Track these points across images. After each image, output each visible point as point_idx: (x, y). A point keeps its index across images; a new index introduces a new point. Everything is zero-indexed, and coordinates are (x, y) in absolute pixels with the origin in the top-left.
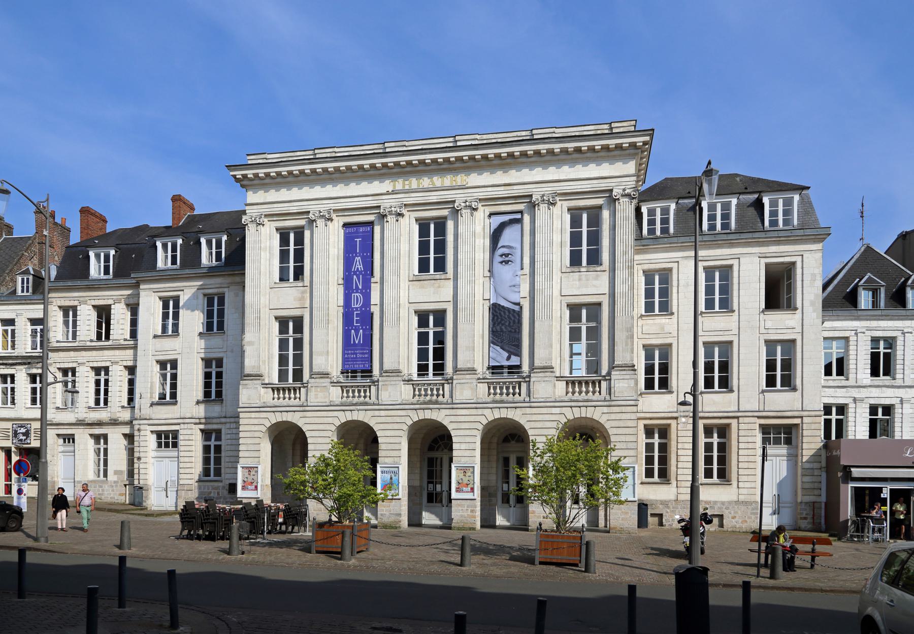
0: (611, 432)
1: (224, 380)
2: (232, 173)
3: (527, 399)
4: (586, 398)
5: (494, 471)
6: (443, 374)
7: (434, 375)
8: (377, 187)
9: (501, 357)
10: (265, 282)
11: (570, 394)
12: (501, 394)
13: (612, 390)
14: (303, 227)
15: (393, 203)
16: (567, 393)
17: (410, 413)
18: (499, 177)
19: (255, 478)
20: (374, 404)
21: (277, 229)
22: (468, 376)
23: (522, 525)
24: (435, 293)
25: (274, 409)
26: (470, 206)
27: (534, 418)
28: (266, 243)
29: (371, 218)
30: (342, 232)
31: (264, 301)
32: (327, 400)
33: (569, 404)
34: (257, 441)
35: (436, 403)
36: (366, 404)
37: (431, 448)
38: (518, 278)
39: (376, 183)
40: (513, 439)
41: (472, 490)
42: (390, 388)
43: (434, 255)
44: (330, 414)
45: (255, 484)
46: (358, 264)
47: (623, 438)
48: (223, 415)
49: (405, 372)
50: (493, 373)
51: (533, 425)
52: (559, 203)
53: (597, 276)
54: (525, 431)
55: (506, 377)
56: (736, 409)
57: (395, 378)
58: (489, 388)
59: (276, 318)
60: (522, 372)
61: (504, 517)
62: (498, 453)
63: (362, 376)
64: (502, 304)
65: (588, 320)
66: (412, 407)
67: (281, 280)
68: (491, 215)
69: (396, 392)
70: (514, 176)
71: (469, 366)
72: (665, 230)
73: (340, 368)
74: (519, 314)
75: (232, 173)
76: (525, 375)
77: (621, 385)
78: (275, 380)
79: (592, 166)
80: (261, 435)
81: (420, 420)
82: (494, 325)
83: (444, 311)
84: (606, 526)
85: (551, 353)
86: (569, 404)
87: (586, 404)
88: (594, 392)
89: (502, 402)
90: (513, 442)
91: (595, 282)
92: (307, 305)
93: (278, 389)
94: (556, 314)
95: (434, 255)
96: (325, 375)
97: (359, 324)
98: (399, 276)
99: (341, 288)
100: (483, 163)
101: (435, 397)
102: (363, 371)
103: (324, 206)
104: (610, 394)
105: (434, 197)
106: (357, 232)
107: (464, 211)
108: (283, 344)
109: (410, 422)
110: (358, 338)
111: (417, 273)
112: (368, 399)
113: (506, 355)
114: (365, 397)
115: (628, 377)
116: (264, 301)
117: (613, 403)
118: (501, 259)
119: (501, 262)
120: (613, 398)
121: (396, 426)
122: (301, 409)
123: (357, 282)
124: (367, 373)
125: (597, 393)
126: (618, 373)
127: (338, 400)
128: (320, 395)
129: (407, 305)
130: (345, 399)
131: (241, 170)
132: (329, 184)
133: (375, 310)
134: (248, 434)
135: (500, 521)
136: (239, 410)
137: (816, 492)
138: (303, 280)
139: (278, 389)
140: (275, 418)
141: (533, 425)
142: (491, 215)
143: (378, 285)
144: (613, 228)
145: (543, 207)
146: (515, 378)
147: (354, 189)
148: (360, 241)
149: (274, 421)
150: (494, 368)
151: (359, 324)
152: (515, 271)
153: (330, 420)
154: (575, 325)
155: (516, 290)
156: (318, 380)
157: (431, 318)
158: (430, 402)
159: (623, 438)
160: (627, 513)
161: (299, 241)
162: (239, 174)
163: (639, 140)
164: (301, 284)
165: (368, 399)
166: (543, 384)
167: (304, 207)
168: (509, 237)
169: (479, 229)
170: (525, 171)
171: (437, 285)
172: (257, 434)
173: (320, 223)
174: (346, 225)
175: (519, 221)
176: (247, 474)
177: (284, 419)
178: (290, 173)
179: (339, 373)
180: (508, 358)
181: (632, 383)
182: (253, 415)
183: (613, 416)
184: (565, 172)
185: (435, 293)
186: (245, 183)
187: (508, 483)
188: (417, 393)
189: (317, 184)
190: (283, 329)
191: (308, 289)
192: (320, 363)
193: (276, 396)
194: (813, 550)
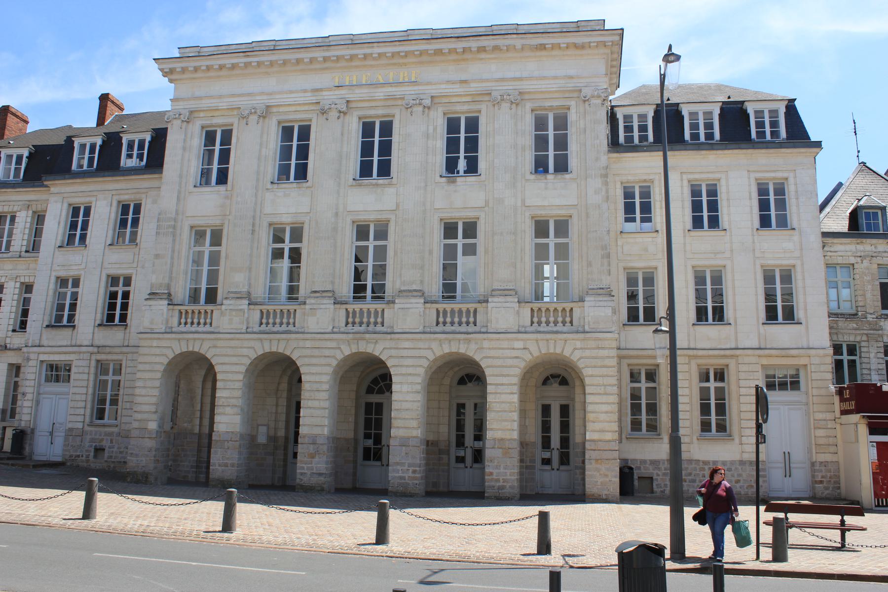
1: (131, 302)
4: (287, 329)
11: (535, 324)
37: (370, 391)
47: (600, 380)
51: (307, 361)
72: (709, 136)
114: (288, 324)
115: (605, 304)
121: (234, 360)
125: (568, 324)
126: (592, 299)
137: (833, 449)
141: (307, 361)
145: (505, 106)
159: (600, 380)
194: (843, 522)
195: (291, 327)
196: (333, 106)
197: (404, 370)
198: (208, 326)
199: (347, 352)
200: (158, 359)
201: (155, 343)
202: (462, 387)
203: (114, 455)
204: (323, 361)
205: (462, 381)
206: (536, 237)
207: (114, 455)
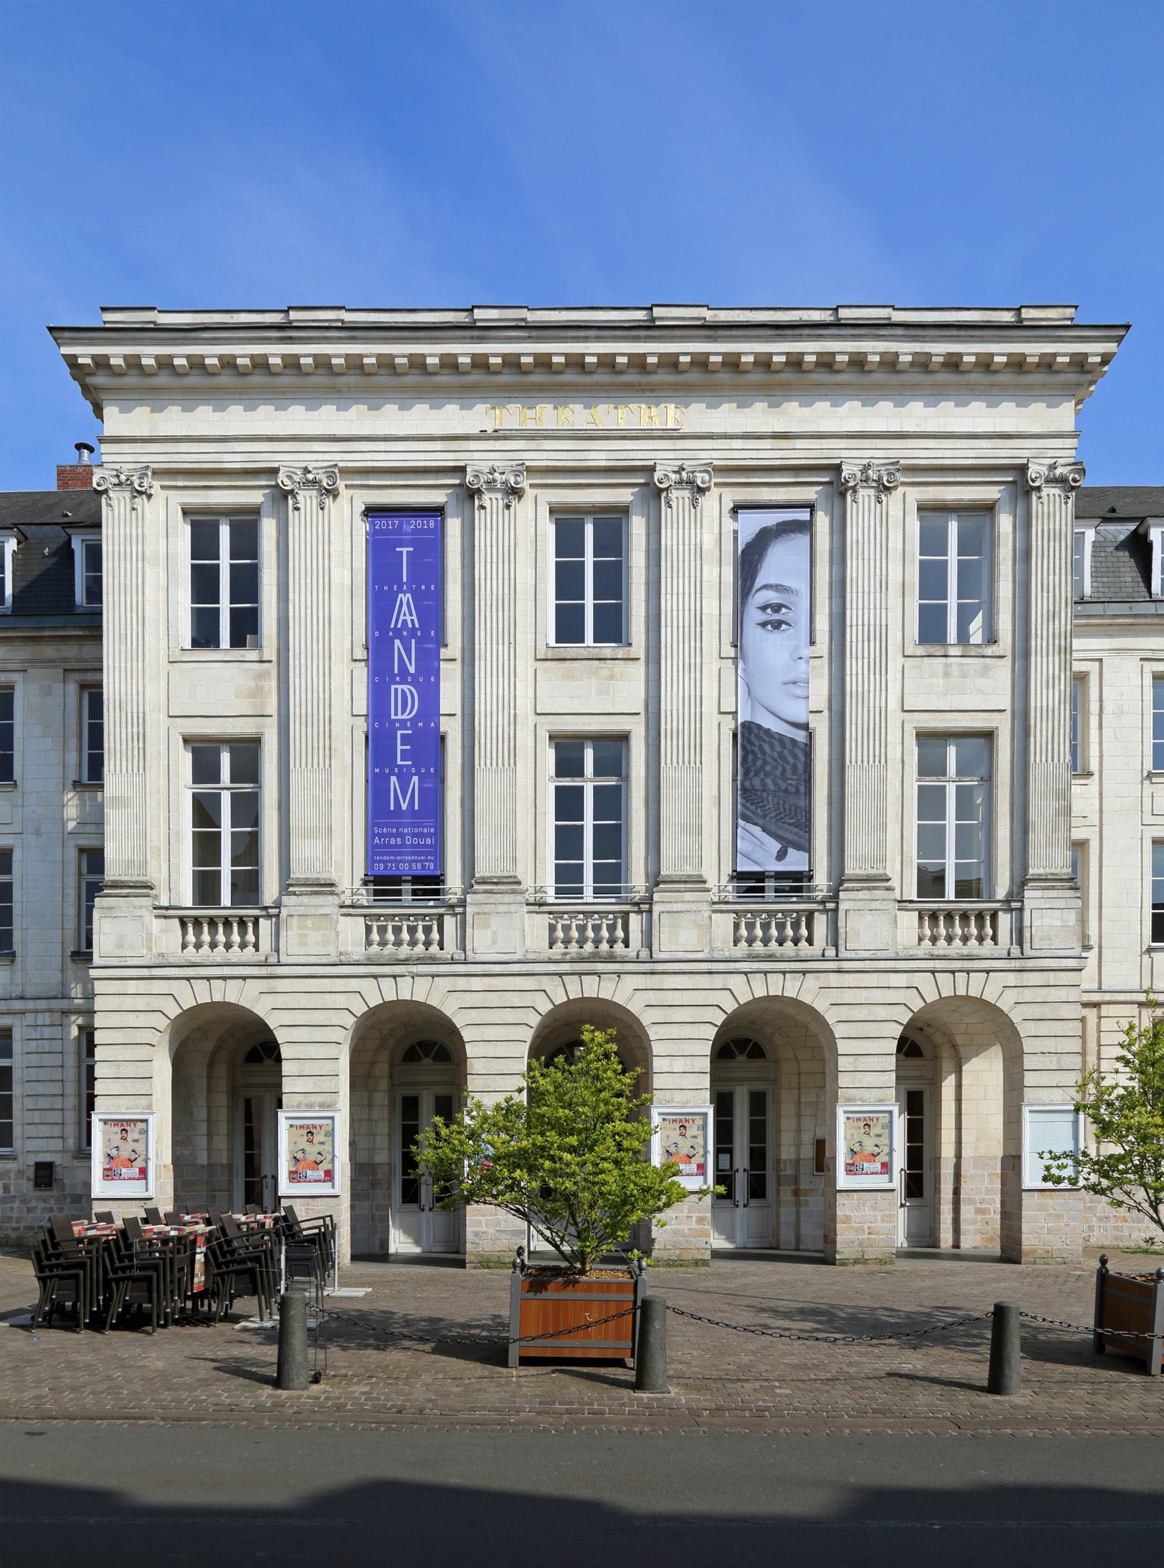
0: (1024, 1030)
2: (66, 350)
3: (831, 953)
5: (383, 1128)
6: (618, 890)
7: (597, 891)
8: (452, 418)
9: (763, 853)
10: (156, 647)
12: (766, 941)
13: (1027, 934)
14: (256, 511)
15: (499, 461)
16: (184, 946)
17: (546, 983)
18: (759, 416)
19: (139, 1147)
20: (453, 961)
21: (185, 512)
22: (688, 896)
23: (450, 1253)
24: (603, 693)
25: (189, 972)
26: (691, 482)
27: (848, 996)
28: (155, 545)
29: (437, 497)
30: (362, 528)
31: (155, 693)
32: (331, 950)
33: (930, 965)
34: (143, 1053)
35: (611, 959)
36: (433, 960)
38: (802, 665)
39: (452, 408)
40: (742, 1052)
41: (329, 1175)
42: (495, 922)
43: (595, 599)
44: (340, 984)
45: (139, 1163)
46: (406, 612)
47: (1050, 1045)
48: (17, 992)
49: (528, 882)
50: (376, 893)
52: (530, 493)
53: (986, 667)
54: (454, 1032)
55: (770, 901)
56: (1095, 986)
57: (507, 898)
58: (368, 929)
59: (187, 740)
60: (630, 890)
61: (408, 1231)
62: (392, 1086)
63: (414, 892)
64: (766, 725)
65: (598, 772)
66: (552, 968)
67: (197, 643)
68: (736, 509)
69: (507, 931)
70: (794, 415)
71: (689, 870)
73: (360, 873)
74: (808, 750)
75: (66, 350)
76: (819, 895)
77: (1047, 921)
78: (186, 896)
79: (978, 406)
80: (153, 1037)
81: (200, 1007)
82: (746, 774)
83: (623, 738)
84: (956, 1245)
85: (883, 844)
86: (930, 965)
87: (967, 965)
89: (770, 958)
90: (427, 1061)
91: (980, 682)
92: (272, 707)
93: (197, 922)
94: (894, 753)
95: (595, 599)
96: (326, 887)
97: (408, 760)
98: (513, 644)
99: (362, 673)
100: (725, 377)
101: (420, 948)
102: (416, 880)
103: (319, 458)
104: (1021, 943)
105: (599, 455)
106: (399, 531)
107: (674, 494)
108: (205, 811)
109: (174, 1011)
110: (405, 796)
111: (553, 643)
112: (434, 949)
113: (776, 846)
115: (1061, 903)
116: (155, 693)
117: (1030, 964)
118: (762, 617)
119: (764, 625)
120: (1028, 952)
121: (511, 1016)
122: (263, 971)
123: (404, 655)
124: (430, 884)
125: (251, 949)
126: (1038, 893)
127: (358, 951)
128: (314, 936)
129: (532, 719)
130: (375, 948)
131: (91, 342)
132: (328, 401)
133: (452, 728)
134: (119, 1037)
135: (399, 1242)
136: (93, 973)
138: (258, 646)
139: (197, 922)
140: (191, 996)
142: (736, 509)
143: (457, 667)
144: (1024, 556)
145: (866, 495)
146: (430, 907)
147: (392, 419)
148: (407, 551)
149: (189, 1003)
150: (378, 880)
151: (408, 760)
152: (797, 648)
153: (340, 1001)
154: (930, 782)
155: (800, 692)
156: (305, 899)
157: (225, 759)
158: (595, 958)
159: (1050, 1045)
160: (1059, 1217)
161: (246, 542)
162: (85, 353)
163: (1094, 349)
164: (252, 655)
165: (434, 949)
166: (869, 917)
168: (782, 564)
169: (709, 540)
170: (822, 406)
171: (605, 673)
172: (141, 1037)
173: (307, 499)
174: (371, 512)
175: (807, 527)
176: (116, 1139)
177: (218, 998)
178: (228, 363)
179: (358, 884)
180: (781, 855)
181: (1071, 918)
182: (132, 987)
183: (1028, 995)
184: (916, 415)
185: (603, 693)
186: (99, 380)
187: (730, 1151)
188: (375, 937)
189: (295, 400)
190: (205, 770)
191: (273, 669)
192: (307, 858)
193: (191, 938)
198: (250, 949)
202: (254, 1067)
203: (15, 1214)
204: (511, 1016)
205: (412, 1055)
207: (15, 1214)
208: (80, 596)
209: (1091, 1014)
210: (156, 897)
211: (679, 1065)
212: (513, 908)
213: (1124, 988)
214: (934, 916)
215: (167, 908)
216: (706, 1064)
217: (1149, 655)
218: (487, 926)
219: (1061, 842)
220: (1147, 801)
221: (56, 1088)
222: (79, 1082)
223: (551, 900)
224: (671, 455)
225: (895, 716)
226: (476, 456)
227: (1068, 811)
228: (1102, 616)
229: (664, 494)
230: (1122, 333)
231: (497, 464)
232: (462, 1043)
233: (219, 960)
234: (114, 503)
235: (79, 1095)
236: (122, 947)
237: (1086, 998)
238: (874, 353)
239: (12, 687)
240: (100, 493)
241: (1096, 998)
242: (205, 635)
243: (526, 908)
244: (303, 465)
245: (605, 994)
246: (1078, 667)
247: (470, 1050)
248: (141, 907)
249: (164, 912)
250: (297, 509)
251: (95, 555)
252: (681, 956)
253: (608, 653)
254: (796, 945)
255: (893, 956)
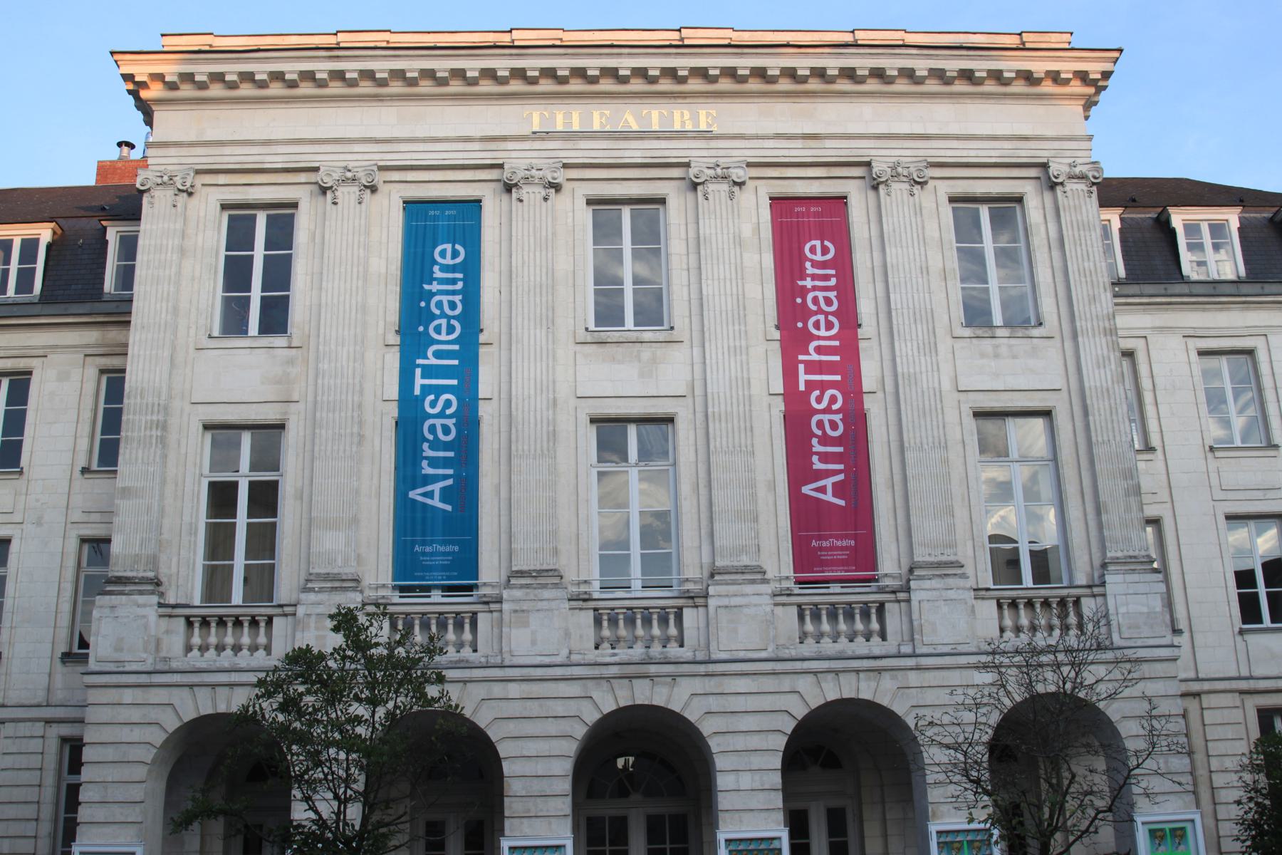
16: (189, 648)
22: (749, 589)
42: (534, 620)
49: (570, 575)
51: (512, 728)
52: (567, 187)
58: (801, 617)
71: (745, 560)
85: (952, 529)
88: (1066, 628)
93: (205, 622)
111: (592, 327)
115: (1141, 588)
121: (552, 727)
126: (1119, 578)
139: (205, 622)
141: (512, 728)
145: (899, 188)
146: (460, 603)
149: (189, 715)
167: (674, 149)
177: (847, 694)
195: (467, 653)
196: (534, 172)
197: (740, 742)
198: (261, 653)
199: (609, 706)
200: (136, 734)
201: (128, 696)
204: (552, 727)
206: (277, 482)
208: (109, 284)
209: (1192, 705)
210: (162, 595)
211: (746, 781)
212: (554, 604)
213: (1221, 675)
214: (1014, 604)
215: (174, 607)
216: (776, 779)
217: (1191, 332)
218: (526, 624)
219: (1136, 522)
220: (1214, 476)
221: (30, 811)
222: (57, 804)
223: (596, 596)
224: (705, 153)
225: (951, 398)
226: (514, 154)
227: (1137, 491)
228: (1141, 296)
229: (700, 188)
230: (1116, 54)
231: (534, 161)
232: (497, 760)
233: (226, 665)
234: (156, 201)
235: (56, 821)
236: (121, 650)
237: (1184, 687)
238: (892, 69)
239: (30, 373)
240: (142, 192)
241: (1195, 687)
242: (234, 322)
243: (567, 605)
244: (344, 164)
245: (658, 701)
246: (1126, 344)
247: (507, 768)
248: (144, 606)
249: (169, 611)
250: (335, 203)
251: (129, 247)
252: (741, 655)
253: (647, 336)
254: (868, 640)
255: (974, 650)
